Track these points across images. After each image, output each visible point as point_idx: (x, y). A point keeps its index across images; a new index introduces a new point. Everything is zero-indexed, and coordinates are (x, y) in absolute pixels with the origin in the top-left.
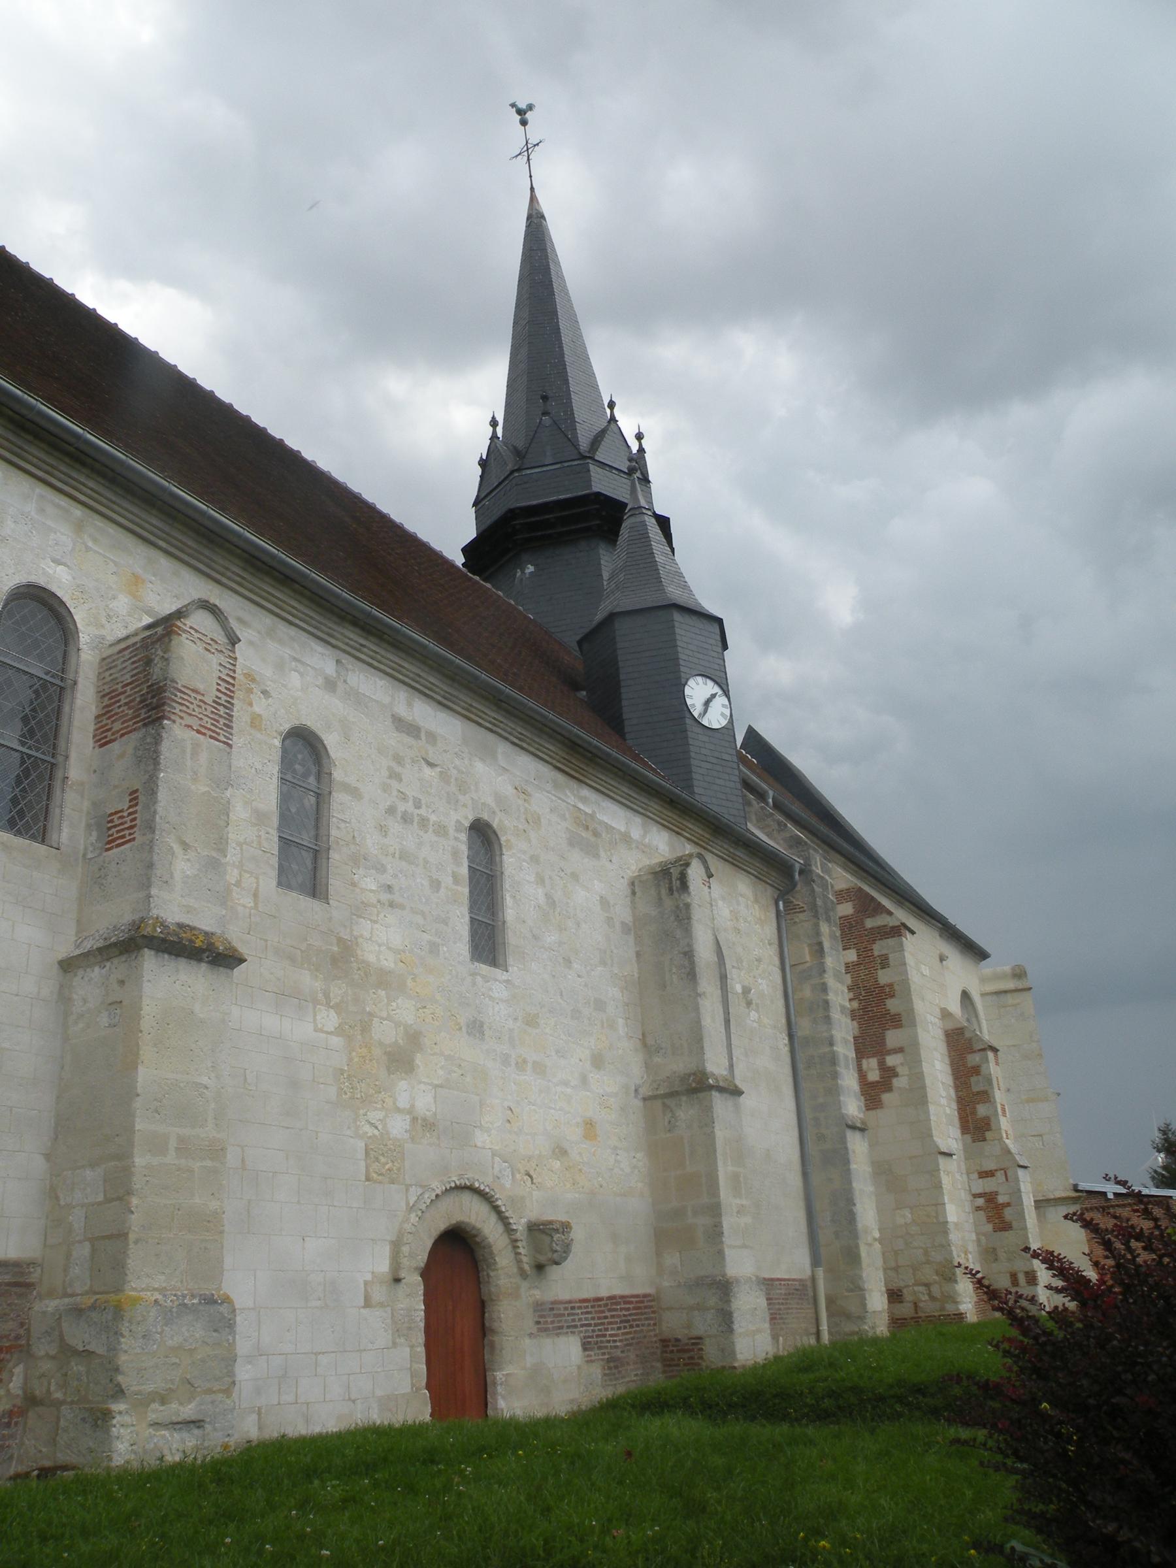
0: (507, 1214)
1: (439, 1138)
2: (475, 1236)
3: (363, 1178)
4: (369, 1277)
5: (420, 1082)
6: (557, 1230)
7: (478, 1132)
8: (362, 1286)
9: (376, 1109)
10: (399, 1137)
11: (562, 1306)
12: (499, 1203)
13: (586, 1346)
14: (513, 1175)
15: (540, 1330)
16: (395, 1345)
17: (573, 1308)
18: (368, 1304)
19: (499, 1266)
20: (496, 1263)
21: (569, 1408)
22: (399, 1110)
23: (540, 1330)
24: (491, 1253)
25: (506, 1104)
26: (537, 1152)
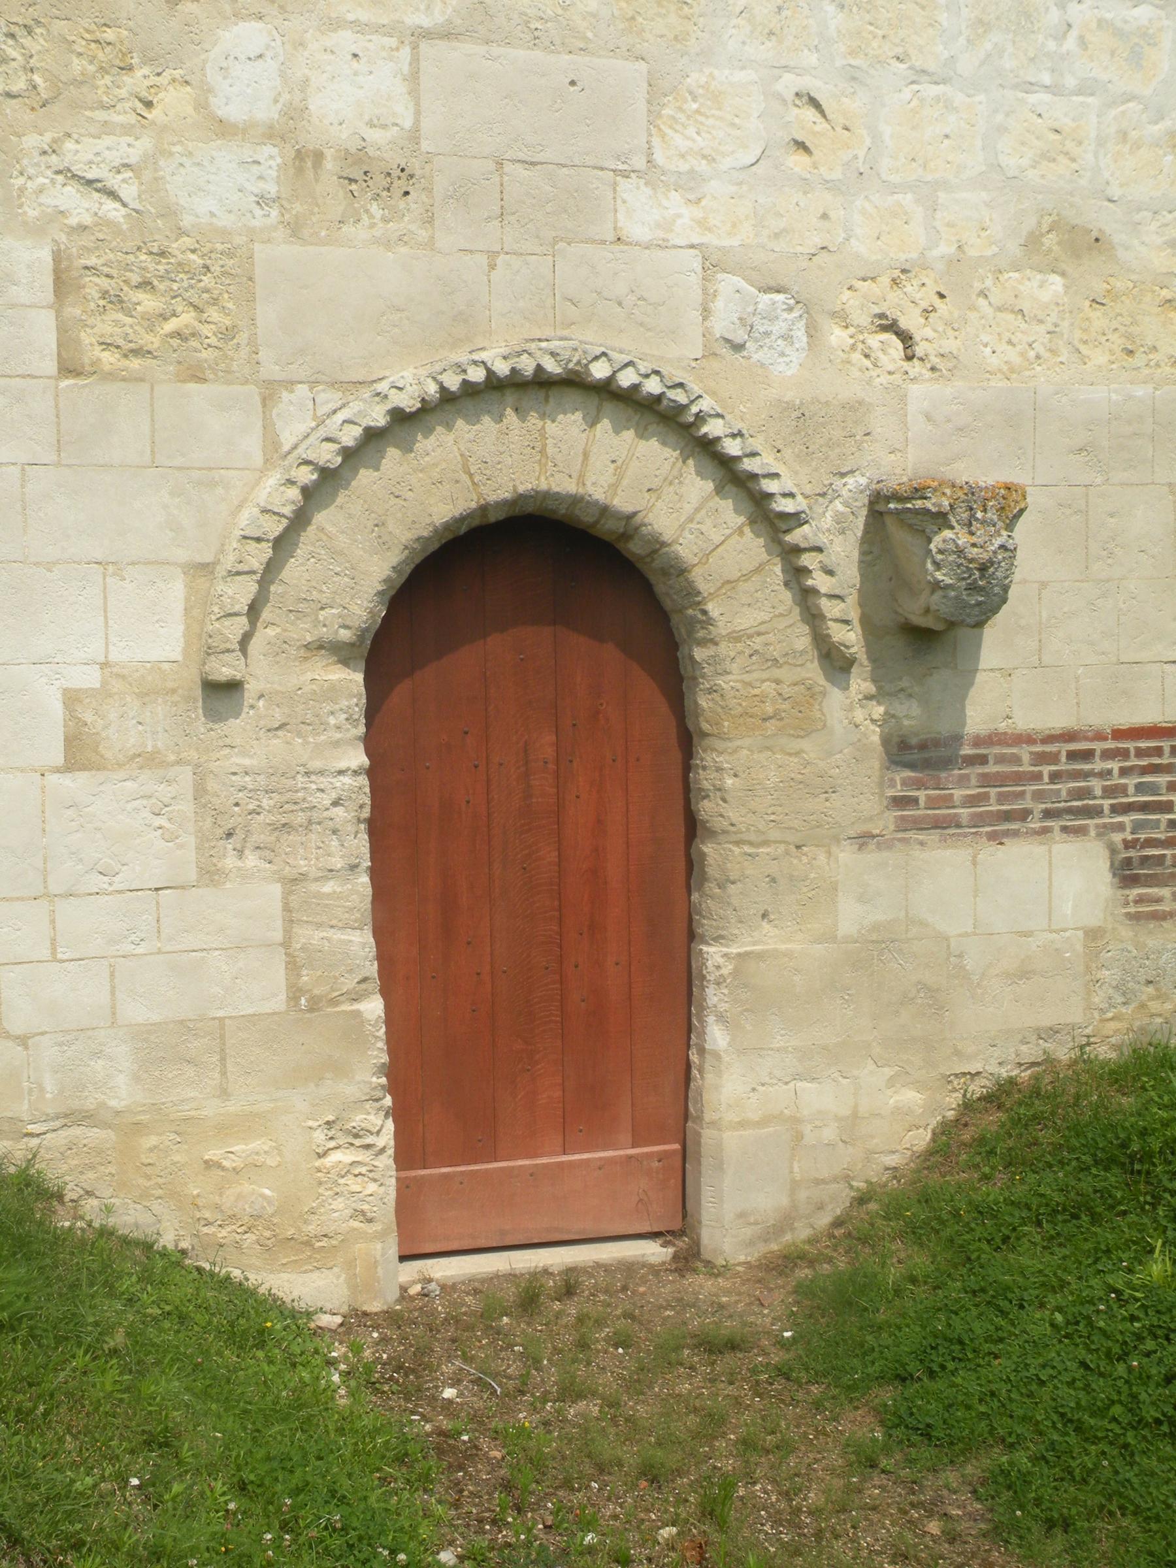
0: (748, 465)
1: (429, 220)
2: (626, 536)
3: (50, 366)
4: (91, 678)
5: (336, 24)
6: (941, 519)
7: (633, 192)
8: (57, 709)
9: (107, 128)
10: (225, 221)
11: (1025, 752)
12: (713, 428)
13: (1127, 873)
14: (812, 331)
15: (904, 825)
16: (211, 875)
17: (1087, 755)
18: (80, 752)
19: (722, 628)
20: (709, 622)
21: (1031, 1052)
22: (223, 129)
23: (904, 825)
24: (691, 592)
25: (788, 84)
26: (946, 249)
